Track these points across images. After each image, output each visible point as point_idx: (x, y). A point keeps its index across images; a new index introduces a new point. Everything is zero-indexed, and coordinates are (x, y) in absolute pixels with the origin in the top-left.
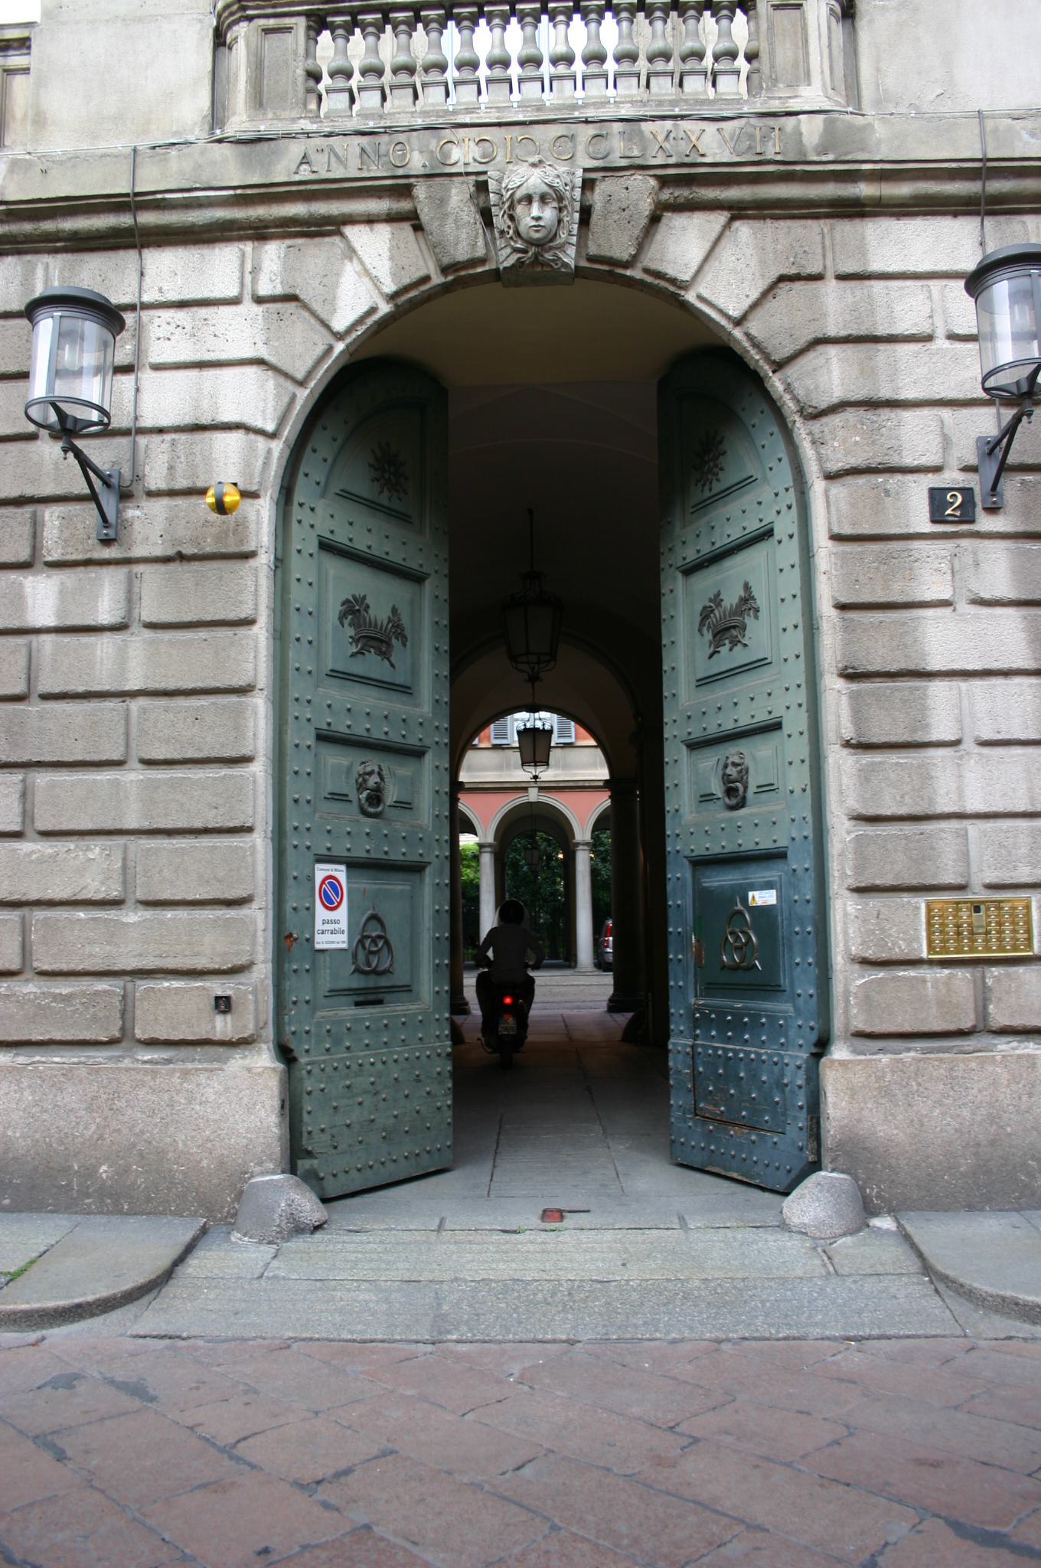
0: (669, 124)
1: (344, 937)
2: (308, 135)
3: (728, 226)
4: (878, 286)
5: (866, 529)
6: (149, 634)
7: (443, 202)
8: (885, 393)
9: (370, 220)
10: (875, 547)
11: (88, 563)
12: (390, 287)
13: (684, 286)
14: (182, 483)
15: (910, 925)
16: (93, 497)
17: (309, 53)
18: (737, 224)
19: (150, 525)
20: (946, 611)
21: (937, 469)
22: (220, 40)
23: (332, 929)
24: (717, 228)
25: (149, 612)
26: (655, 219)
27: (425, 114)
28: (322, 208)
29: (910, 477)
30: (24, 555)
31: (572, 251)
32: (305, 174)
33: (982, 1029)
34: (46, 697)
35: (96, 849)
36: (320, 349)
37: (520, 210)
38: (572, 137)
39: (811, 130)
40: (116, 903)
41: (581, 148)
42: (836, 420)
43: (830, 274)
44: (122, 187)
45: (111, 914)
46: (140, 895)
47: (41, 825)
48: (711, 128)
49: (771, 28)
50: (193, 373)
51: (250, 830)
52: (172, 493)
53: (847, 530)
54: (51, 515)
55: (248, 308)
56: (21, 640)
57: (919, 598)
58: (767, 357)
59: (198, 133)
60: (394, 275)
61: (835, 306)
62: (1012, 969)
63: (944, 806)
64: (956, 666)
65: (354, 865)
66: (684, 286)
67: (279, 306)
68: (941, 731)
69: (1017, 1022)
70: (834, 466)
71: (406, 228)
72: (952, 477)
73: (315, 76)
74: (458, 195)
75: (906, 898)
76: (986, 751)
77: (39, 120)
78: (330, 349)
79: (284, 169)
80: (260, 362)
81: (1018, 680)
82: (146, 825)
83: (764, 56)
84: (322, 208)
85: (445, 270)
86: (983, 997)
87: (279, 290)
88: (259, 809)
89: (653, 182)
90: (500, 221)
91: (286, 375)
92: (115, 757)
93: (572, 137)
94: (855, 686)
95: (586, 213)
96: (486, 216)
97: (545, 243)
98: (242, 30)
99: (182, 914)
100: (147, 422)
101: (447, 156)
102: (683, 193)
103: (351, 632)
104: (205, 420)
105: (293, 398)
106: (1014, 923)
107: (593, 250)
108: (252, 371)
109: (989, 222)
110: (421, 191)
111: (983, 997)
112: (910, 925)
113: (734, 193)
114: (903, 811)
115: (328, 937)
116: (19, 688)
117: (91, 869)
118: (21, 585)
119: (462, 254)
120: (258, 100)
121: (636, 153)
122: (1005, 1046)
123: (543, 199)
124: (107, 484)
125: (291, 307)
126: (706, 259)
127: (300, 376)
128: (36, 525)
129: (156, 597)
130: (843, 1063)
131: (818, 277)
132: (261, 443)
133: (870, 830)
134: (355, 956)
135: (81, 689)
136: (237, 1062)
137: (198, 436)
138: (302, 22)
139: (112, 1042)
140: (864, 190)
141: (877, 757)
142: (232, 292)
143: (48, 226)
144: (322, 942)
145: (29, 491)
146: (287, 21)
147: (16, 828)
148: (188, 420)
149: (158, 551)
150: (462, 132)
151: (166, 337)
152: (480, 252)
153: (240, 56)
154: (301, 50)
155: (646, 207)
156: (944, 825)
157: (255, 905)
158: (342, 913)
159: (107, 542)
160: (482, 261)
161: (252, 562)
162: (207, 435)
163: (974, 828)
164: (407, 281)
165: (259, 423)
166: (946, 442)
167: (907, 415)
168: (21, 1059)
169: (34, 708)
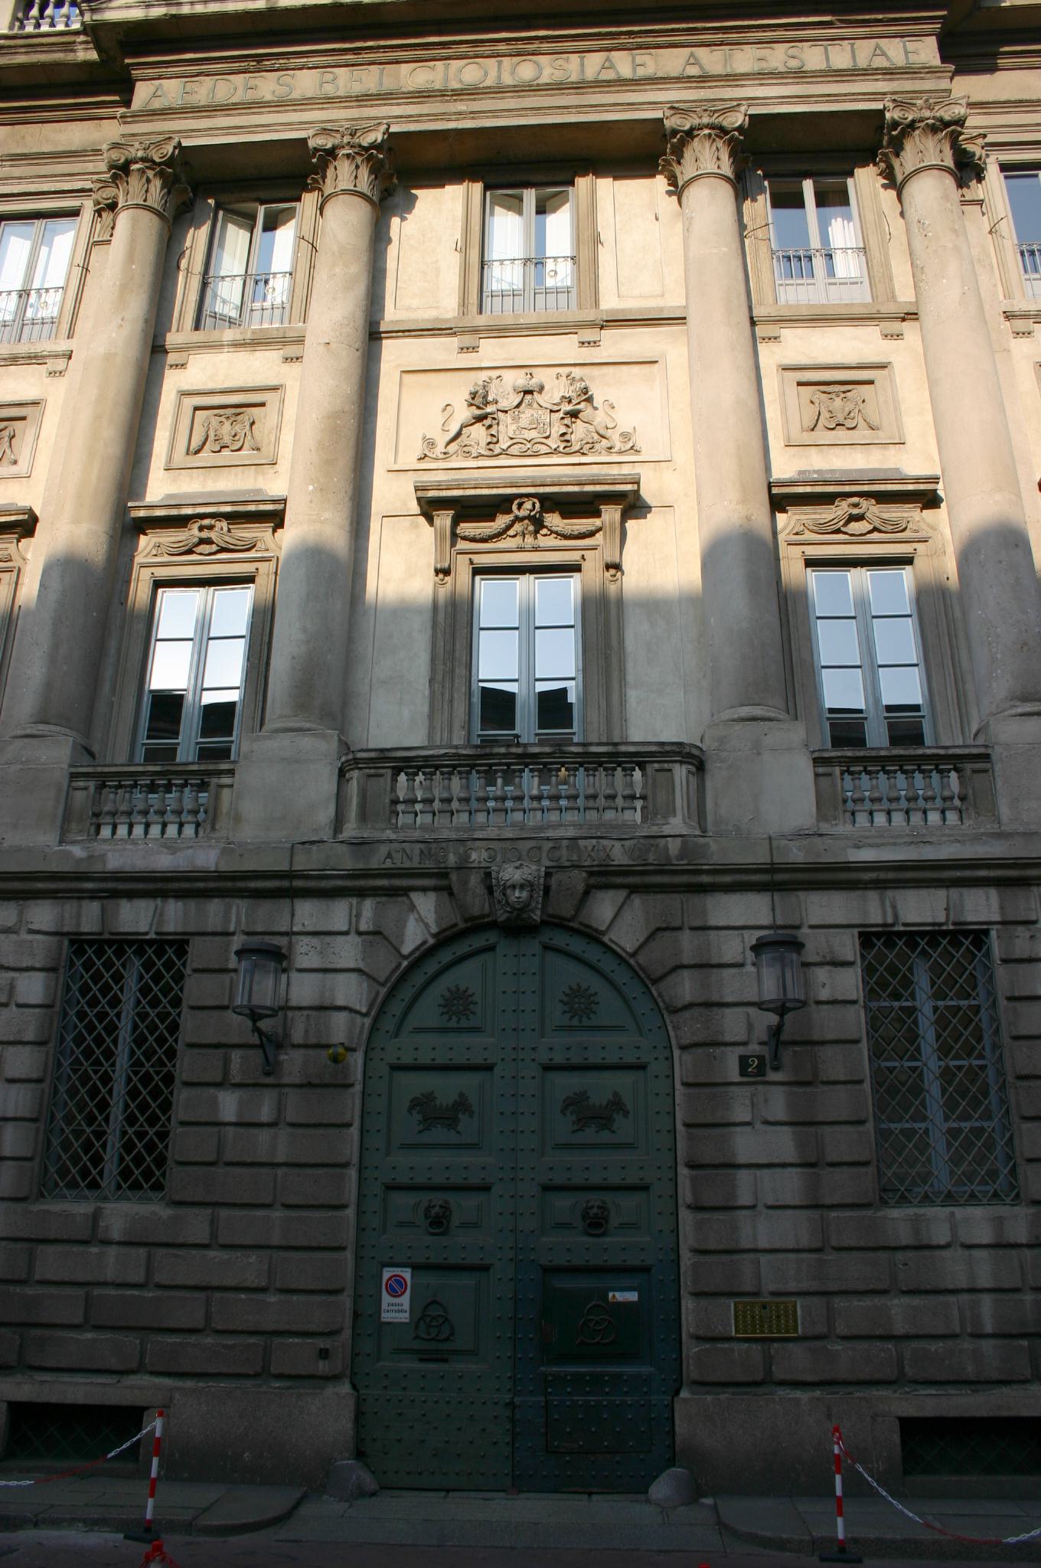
0: (594, 841)
1: (407, 1315)
2: (391, 841)
3: (628, 897)
4: (712, 933)
5: (702, 1080)
6: (289, 1130)
7: (465, 883)
8: (715, 998)
9: (424, 889)
10: (707, 1090)
11: (255, 1085)
12: (434, 929)
13: (603, 933)
14: (313, 1041)
15: (726, 1316)
16: (261, 1046)
17: (393, 789)
18: (633, 896)
19: (293, 1064)
20: (748, 1129)
21: (745, 1044)
22: (342, 773)
23: (396, 1309)
24: (621, 900)
25: (291, 1115)
26: (586, 893)
27: (458, 829)
28: (397, 882)
29: (729, 1048)
30: (219, 1078)
31: (538, 912)
32: (388, 864)
33: (767, 1381)
34: (228, 1164)
35: (253, 1257)
36: (394, 965)
37: (509, 891)
38: (539, 848)
39: (674, 846)
40: (263, 1290)
41: (544, 855)
42: (687, 1014)
43: (686, 926)
44: (285, 867)
45: (261, 1296)
46: (278, 1285)
47: (221, 1241)
48: (618, 844)
49: (654, 781)
50: (319, 975)
51: (344, 1249)
52: (306, 1046)
53: (691, 1080)
54: (236, 1056)
55: (353, 938)
56: (215, 1129)
57: (732, 1120)
58: (648, 977)
59: (326, 835)
60: (437, 922)
61: (688, 944)
62: (786, 1345)
63: (745, 1244)
64: (753, 1161)
65: (415, 1268)
66: (603, 933)
67: (371, 937)
68: (745, 1199)
69: (789, 1377)
70: (685, 1042)
71: (445, 894)
72: (754, 1048)
73: (395, 802)
74: (474, 880)
75: (723, 1300)
76: (770, 1212)
77: (237, 819)
78: (400, 964)
79: (377, 860)
80: (358, 970)
81: (790, 1169)
82: (283, 1243)
83: (650, 798)
84: (397, 882)
85: (466, 921)
86: (768, 1361)
87: (371, 928)
88: (349, 1235)
89: (584, 874)
90: (497, 894)
91: (374, 979)
92: (268, 1201)
93: (539, 848)
94: (694, 1172)
95: (547, 890)
96: (490, 890)
97: (526, 906)
98: (355, 774)
99: (302, 1298)
100: (293, 1003)
101: (469, 857)
102: (603, 880)
103: (420, 1117)
104: (327, 1003)
105: (378, 993)
106: (787, 1316)
107: (550, 911)
108: (354, 976)
109: (777, 896)
110: (454, 877)
111: (768, 1361)
112: (726, 1316)
113: (631, 880)
114: (721, 1247)
115: (390, 1315)
116: (212, 1158)
117: (250, 1268)
118: (216, 1097)
119: (476, 911)
120: (363, 817)
121: (575, 858)
122: (782, 1392)
123: (522, 887)
124: (270, 1041)
125: (378, 938)
126: (615, 917)
127: (382, 980)
128: (227, 1061)
129: (295, 1107)
130: (684, 1400)
131: (680, 929)
132: (359, 1019)
133: (702, 1258)
134: (417, 1327)
135: (249, 1160)
136: (330, 1390)
137: (323, 1013)
138: (389, 772)
139: (256, 1375)
140: (705, 879)
141: (707, 1215)
142: (345, 928)
143: (241, 884)
144: (386, 1317)
145: (224, 1040)
146: (382, 771)
147: (207, 1242)
148: (317, 1003)
149: (297, 1081)
150: (478, 843)
151: (306, 954)
152: (487, 910)
153: (353, 787)
154: (389, 788)
155: (581, 888)
156: (745, 1256)
157: (346, 1293)
158: (405, 1300)
159: (268, 1074)
160: (488, 916)
161: (351, 1090)
162: (328, 1013)
163: (764, 1259)
164: (444, 926)
165: (358, 1008)
166: (750, 1027)
167: (728, 1011)
168: (201, 1384)
169: (221, 1170)
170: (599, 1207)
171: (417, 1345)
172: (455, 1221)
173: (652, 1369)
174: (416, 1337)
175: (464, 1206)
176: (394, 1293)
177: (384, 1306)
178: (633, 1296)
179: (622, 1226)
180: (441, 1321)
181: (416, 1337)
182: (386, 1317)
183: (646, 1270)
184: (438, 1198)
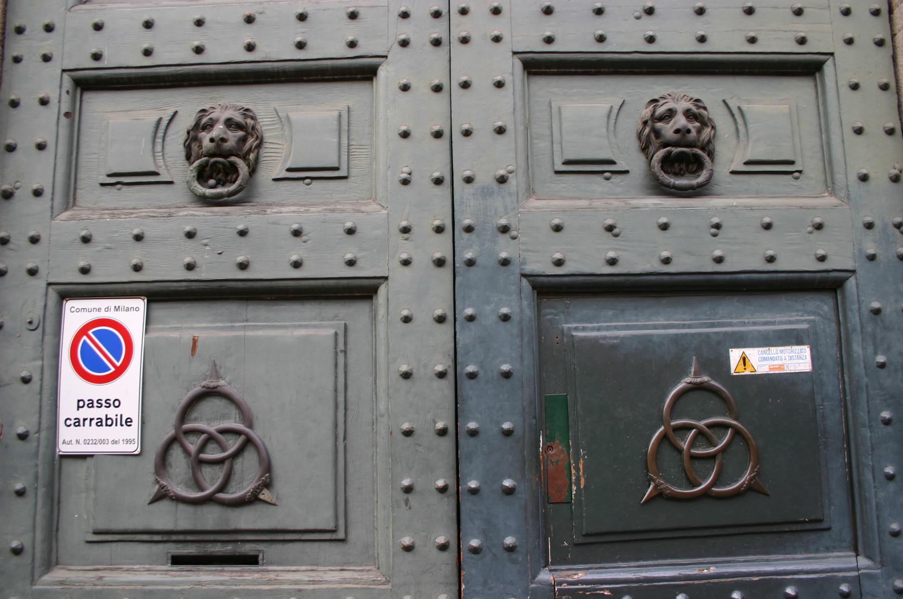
1: (134, 432)
144: (70, 440)
158: (127, 388)
170: (688, 114)
171: (165, 517)
172: (273, 164)
173: (863, 561)
174: (161, 496)
175: (294, 124)
176: (94, 370)
177: (67, 409)
178: (796, 360)
179: (757, 167)
180: (233, 444)
181: (161, 496)
182: (70, 440)
183: (827, 285)
184: (679, 92)
